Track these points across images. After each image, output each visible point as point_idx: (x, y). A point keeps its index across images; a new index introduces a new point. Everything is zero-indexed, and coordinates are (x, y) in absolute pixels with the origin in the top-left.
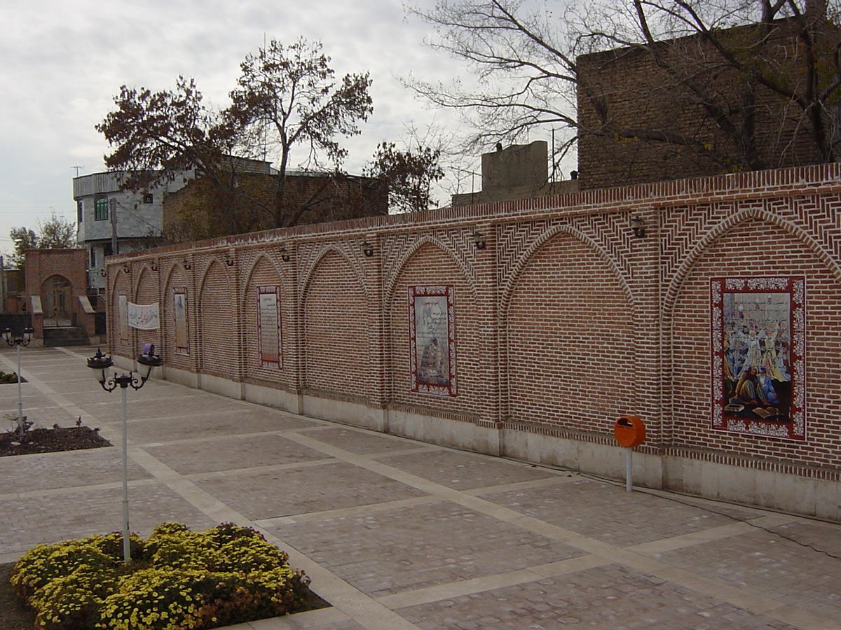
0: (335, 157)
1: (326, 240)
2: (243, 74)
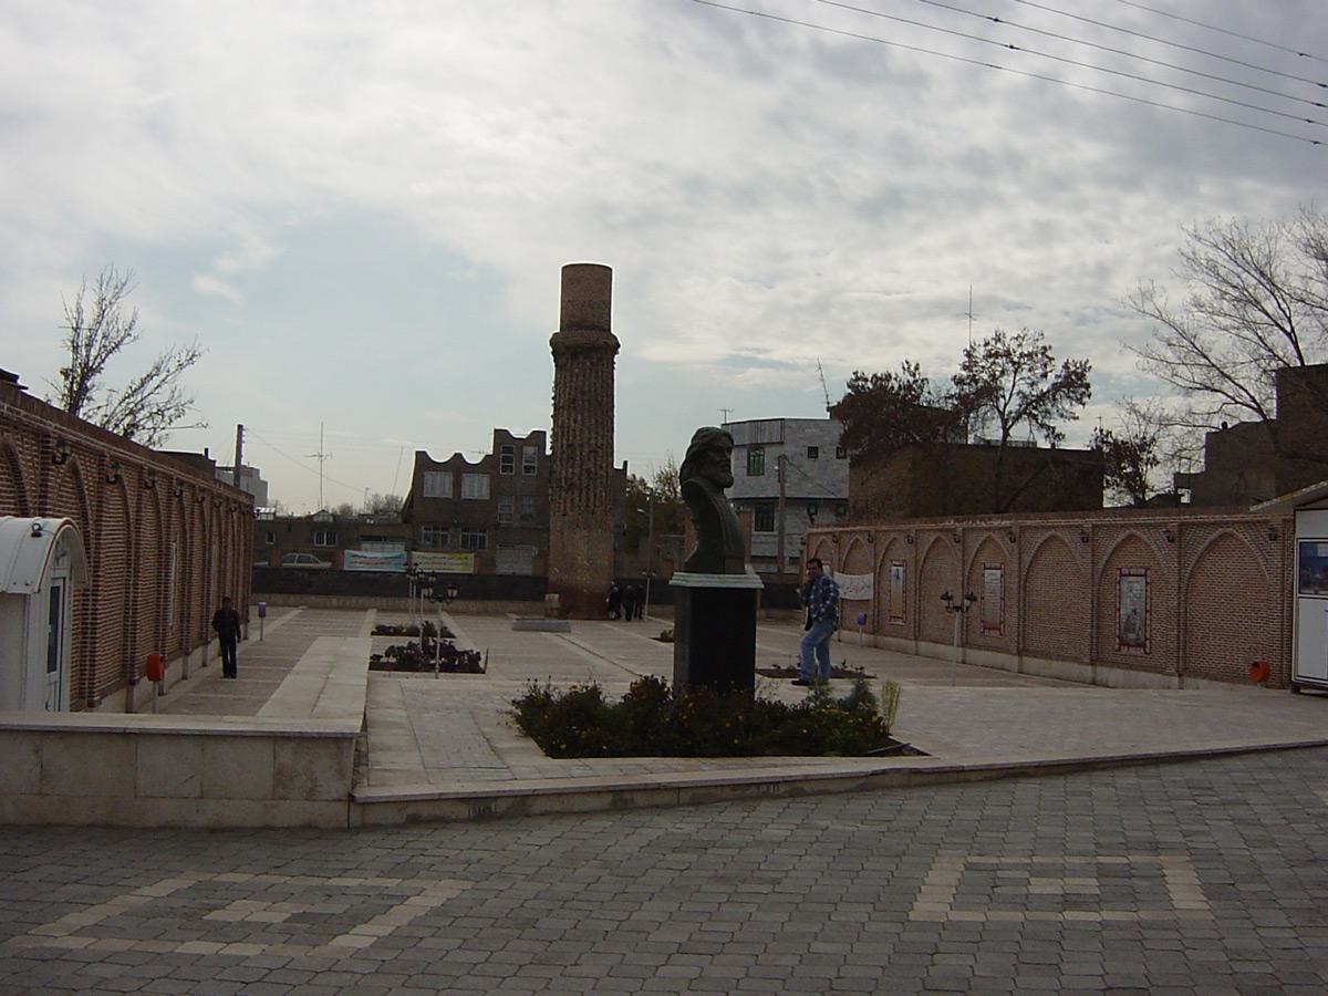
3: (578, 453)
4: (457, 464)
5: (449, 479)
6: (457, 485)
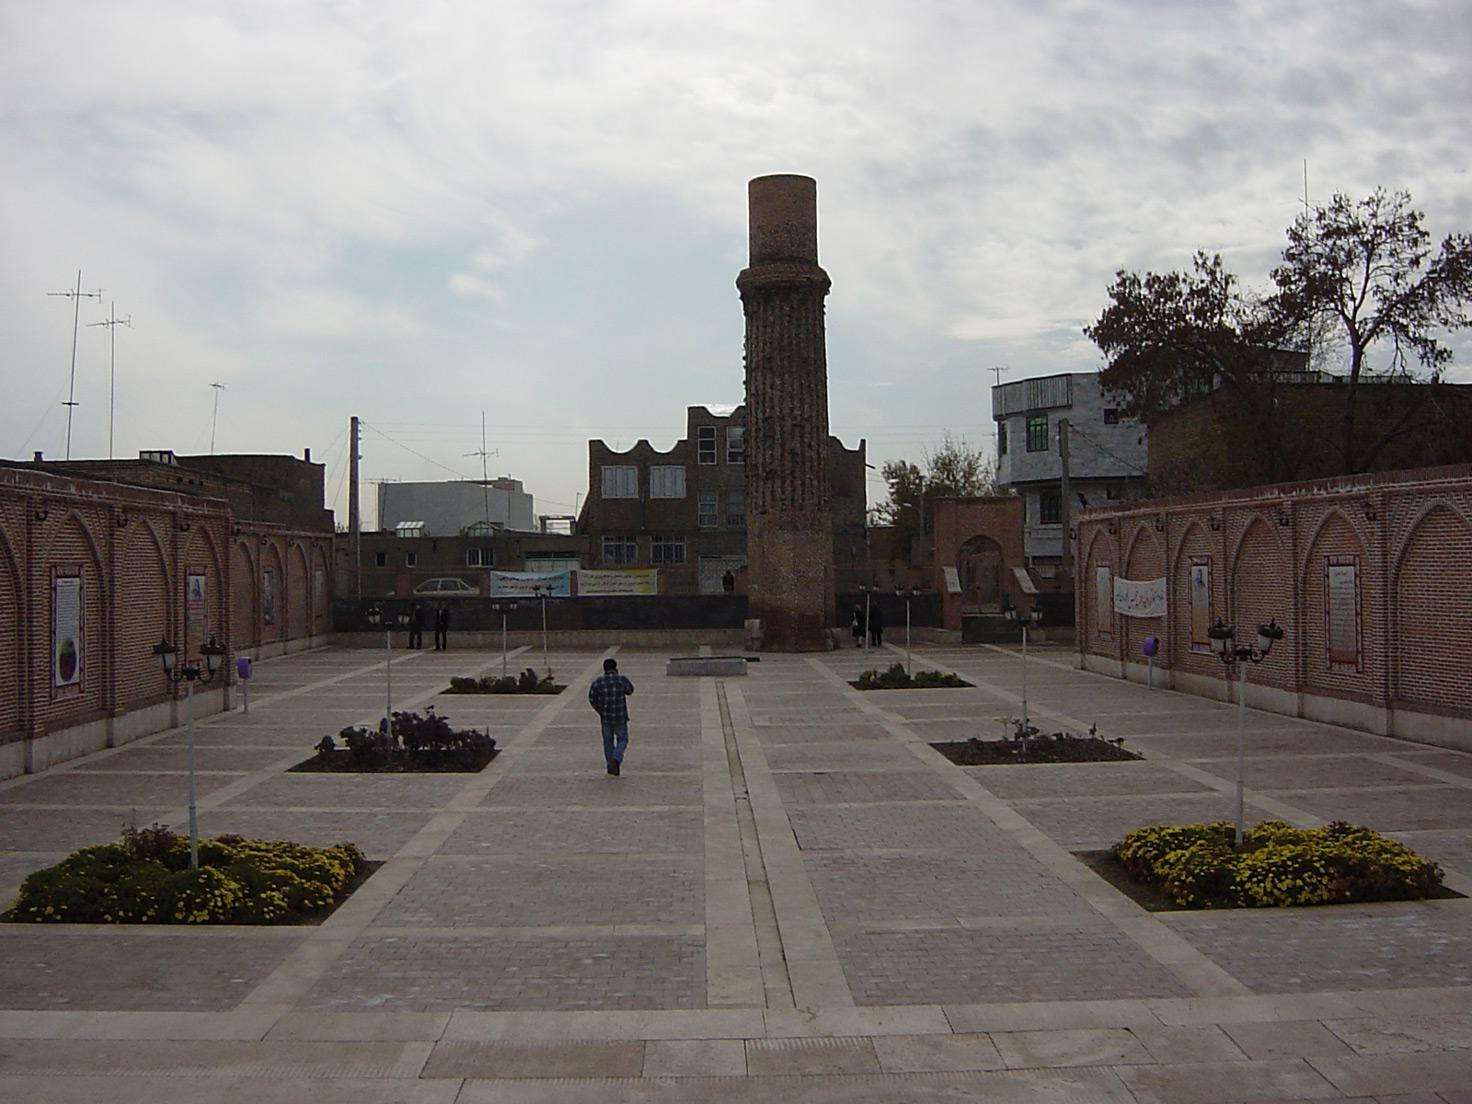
0: (1431, 360)
1: (1432, 491)
2: (1292, 244)
5: (633, 473)
6: (644, 481)
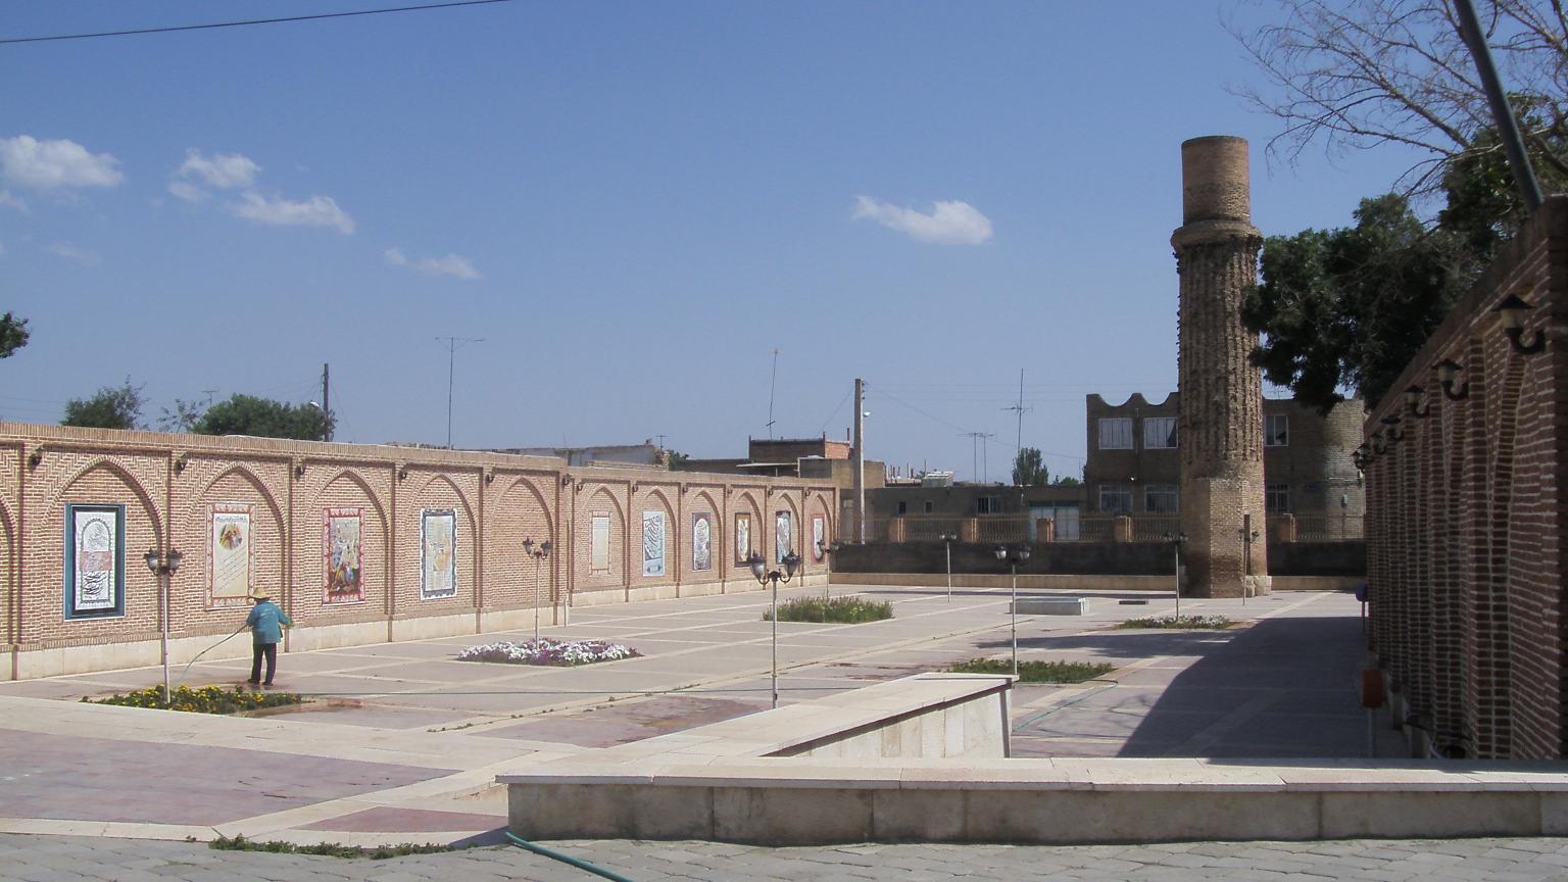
3: (1202, 381)
4: (1136, 406)
5: (1127, 424)
6: (1138, 433)
